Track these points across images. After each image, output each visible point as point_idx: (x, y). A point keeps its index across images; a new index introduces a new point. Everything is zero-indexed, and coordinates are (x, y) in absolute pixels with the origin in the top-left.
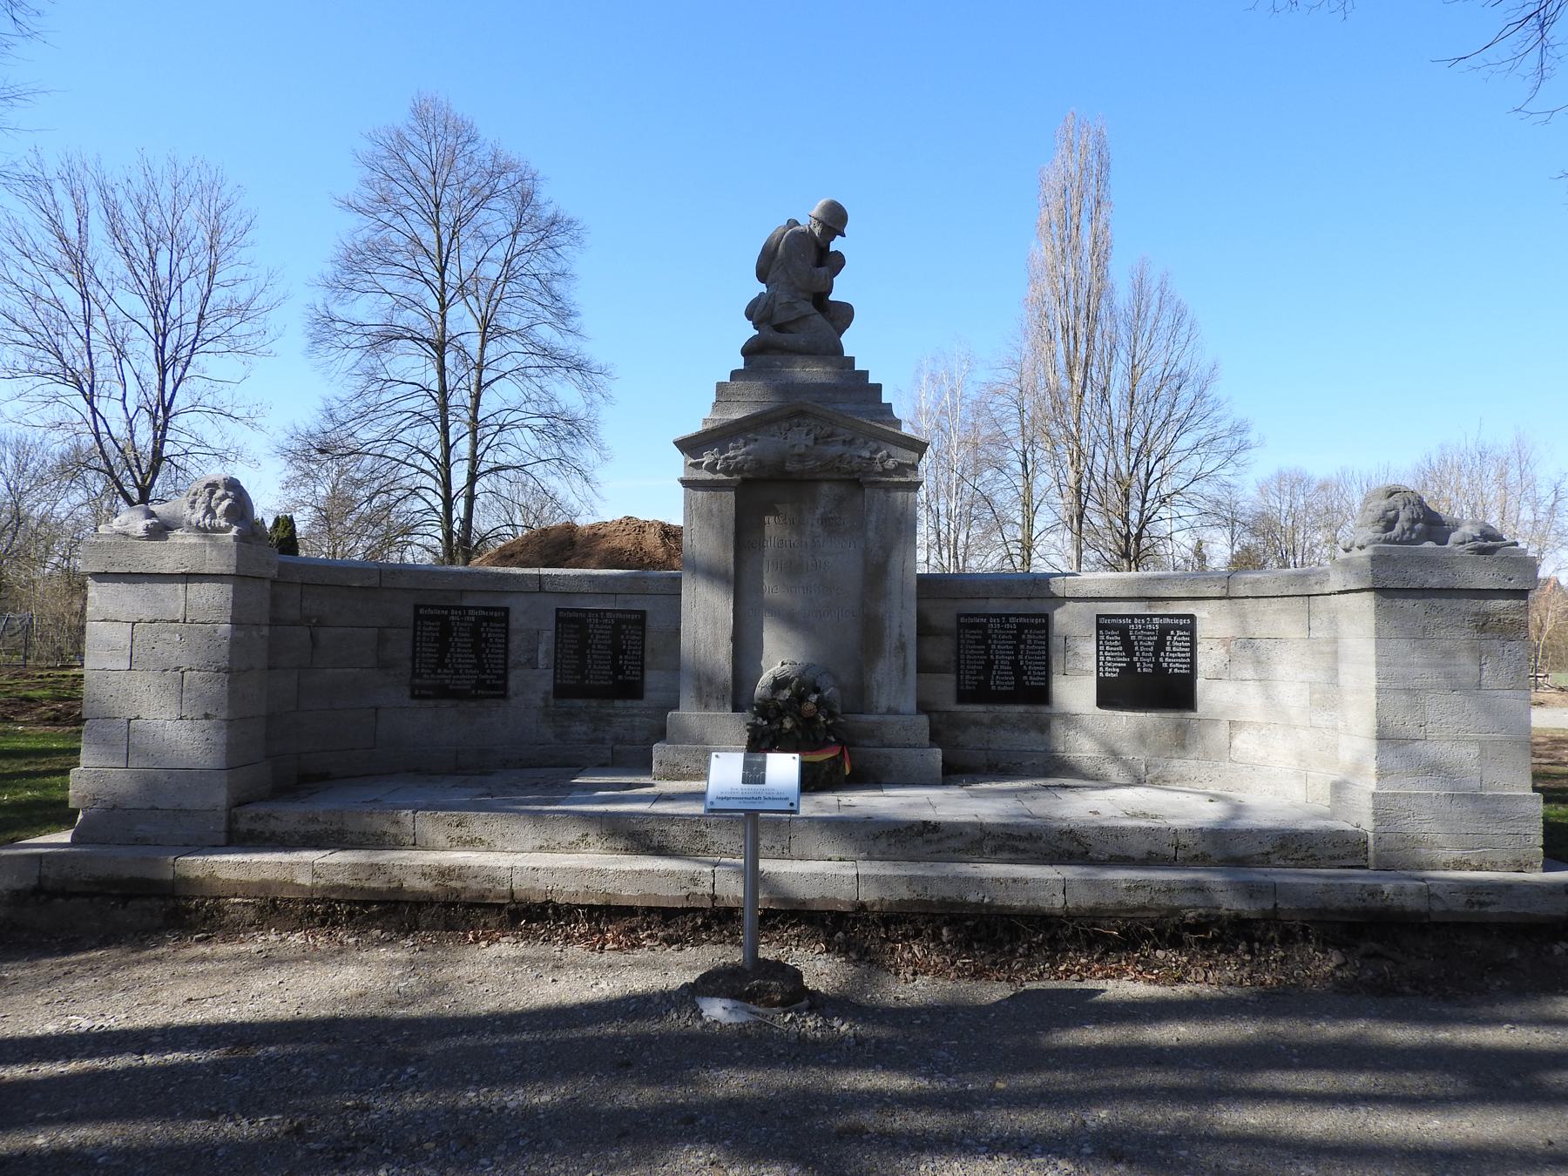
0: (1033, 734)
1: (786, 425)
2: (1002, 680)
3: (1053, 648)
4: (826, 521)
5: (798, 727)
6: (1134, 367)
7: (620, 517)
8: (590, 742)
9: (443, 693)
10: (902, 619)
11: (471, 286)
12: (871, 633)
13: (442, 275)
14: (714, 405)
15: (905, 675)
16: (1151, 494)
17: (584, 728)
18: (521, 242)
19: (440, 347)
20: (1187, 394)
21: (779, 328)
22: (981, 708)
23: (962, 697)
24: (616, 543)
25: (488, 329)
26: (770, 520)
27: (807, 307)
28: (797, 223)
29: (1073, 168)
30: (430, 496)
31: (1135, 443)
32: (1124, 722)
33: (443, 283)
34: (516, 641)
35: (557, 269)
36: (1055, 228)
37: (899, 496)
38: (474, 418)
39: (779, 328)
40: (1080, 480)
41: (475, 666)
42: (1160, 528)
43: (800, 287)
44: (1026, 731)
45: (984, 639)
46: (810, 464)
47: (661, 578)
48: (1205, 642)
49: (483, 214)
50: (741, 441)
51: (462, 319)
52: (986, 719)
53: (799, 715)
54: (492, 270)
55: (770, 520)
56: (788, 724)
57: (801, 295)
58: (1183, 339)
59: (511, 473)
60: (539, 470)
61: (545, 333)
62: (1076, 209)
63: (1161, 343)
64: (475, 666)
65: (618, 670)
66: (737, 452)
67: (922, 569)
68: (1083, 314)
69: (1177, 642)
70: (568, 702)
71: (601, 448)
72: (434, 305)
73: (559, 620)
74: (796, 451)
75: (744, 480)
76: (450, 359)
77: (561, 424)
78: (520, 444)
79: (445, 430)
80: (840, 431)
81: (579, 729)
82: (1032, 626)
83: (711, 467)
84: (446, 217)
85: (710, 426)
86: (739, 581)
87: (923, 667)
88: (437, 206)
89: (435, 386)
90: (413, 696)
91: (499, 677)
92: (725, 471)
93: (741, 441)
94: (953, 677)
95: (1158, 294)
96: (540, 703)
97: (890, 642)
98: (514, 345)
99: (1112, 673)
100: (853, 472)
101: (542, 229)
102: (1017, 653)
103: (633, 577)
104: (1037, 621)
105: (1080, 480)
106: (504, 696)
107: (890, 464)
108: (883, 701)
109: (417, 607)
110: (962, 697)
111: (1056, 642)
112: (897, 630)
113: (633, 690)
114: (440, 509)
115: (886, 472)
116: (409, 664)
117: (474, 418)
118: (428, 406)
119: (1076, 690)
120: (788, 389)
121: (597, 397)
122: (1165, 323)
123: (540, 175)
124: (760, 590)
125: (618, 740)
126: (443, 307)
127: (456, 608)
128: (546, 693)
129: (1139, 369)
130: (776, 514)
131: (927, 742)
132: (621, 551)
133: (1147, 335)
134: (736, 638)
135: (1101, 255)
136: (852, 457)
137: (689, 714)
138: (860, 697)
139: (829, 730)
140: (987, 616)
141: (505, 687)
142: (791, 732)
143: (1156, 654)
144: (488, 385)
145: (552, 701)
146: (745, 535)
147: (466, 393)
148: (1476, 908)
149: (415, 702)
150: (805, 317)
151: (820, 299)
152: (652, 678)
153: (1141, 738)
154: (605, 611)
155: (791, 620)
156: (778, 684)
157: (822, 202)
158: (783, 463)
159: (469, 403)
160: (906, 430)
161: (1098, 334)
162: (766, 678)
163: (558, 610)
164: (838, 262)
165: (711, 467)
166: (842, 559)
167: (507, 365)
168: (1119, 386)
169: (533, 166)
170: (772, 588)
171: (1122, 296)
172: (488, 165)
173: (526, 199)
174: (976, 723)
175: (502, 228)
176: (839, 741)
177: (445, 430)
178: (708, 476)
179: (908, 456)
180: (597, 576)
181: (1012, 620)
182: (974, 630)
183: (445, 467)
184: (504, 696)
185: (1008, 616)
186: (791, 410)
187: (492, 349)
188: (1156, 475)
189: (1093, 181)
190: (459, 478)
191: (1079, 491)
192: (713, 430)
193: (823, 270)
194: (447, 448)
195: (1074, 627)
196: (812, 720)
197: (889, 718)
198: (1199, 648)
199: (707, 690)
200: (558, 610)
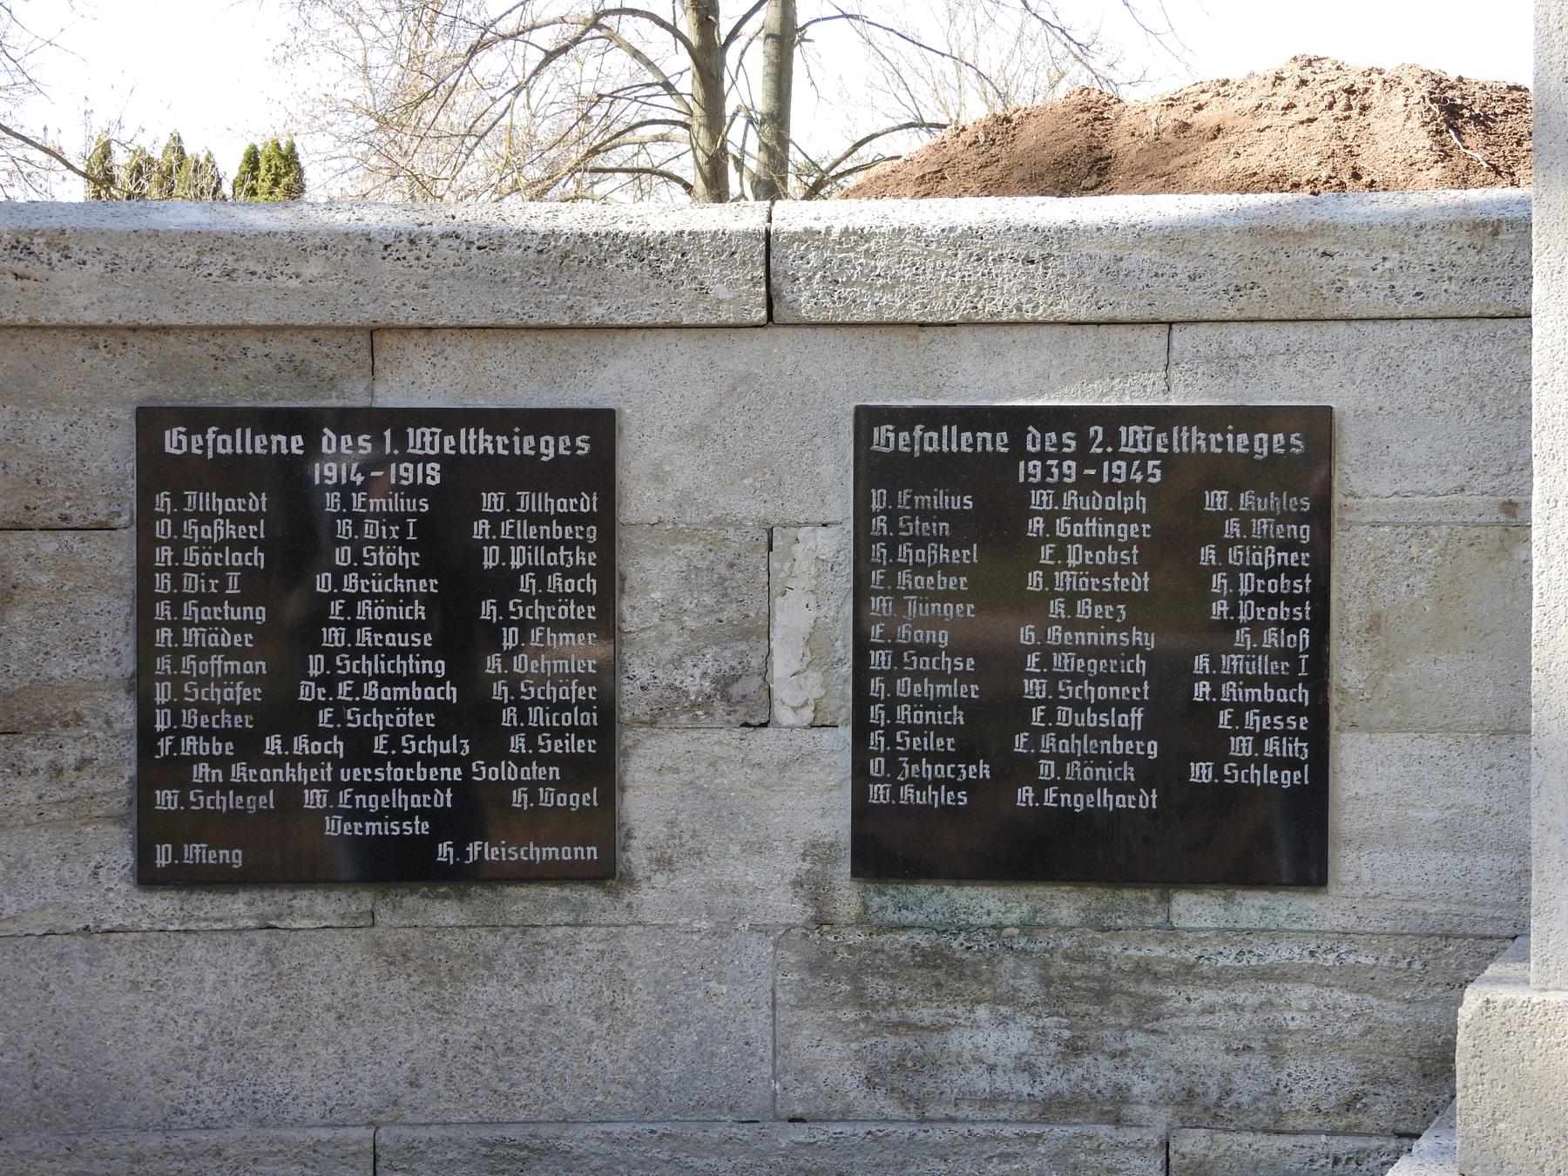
7: (1277, 59)
8: (1055, 1108)
9: (278, 855)
17: (1018, 1039)
34: (653, 585)
41: (447, 720)
64: (447, 720)
65: (1185, 724)
70: (937, 901)
73: (873, 470)
81: (992, 1041)
90: (148, 877)
91: (578, 772)
96: (795, 910)
104: (550, 448)
106: (605, 872)
109: (151, 421)
113: (1284, 839)
114: (687, 84)
116: (125, 712)
125: (1194, 1104)
127: (348, 420)
128: (816, 850)
141: (604, 826)
145: (847, 895)
149: (163, 904)
152: (1369, 775)
163: (867, 419)
181: (1133, 437)
184: (605, 872)
200: (867, 419)
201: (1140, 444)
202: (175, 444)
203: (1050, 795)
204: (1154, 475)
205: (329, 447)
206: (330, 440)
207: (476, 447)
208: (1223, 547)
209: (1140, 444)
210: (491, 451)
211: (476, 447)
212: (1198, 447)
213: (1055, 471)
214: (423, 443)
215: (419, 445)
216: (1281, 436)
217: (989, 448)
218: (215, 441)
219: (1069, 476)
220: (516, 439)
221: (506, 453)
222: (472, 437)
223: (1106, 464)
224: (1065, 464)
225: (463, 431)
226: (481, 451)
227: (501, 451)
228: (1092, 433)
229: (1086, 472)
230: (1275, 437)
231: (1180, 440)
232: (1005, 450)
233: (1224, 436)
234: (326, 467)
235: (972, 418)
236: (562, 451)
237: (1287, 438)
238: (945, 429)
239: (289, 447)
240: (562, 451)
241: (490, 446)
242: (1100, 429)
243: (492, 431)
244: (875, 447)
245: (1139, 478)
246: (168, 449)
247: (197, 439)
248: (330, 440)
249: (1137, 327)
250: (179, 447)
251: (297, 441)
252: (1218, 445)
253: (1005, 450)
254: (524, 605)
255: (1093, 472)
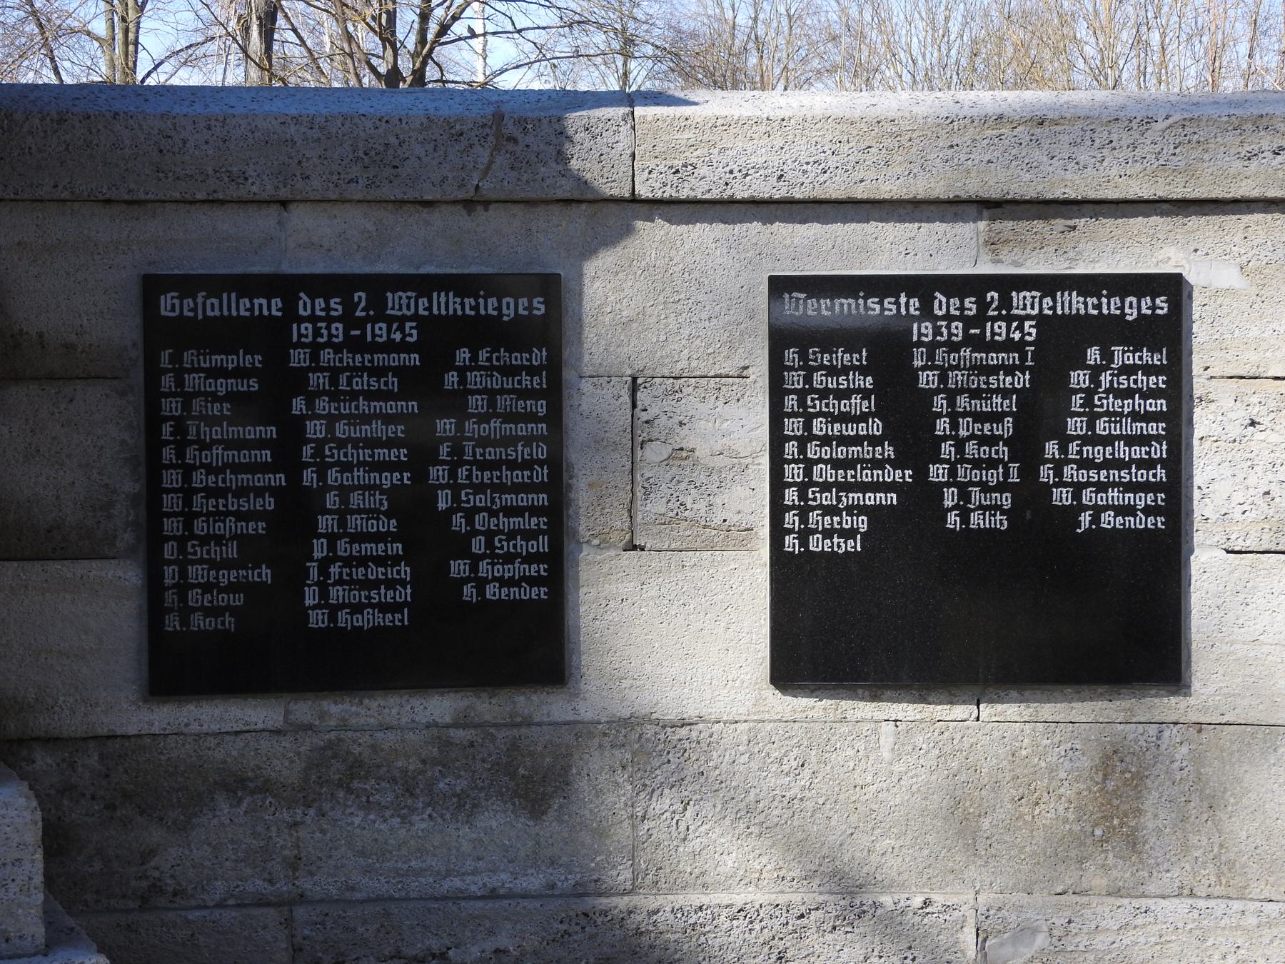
0: (498, 822)
2: (356, 592)
3: (578, 431)
22: (258, 713)
23: (179, 665)
32: (897, 755)
44: (464, 805)
45: (276, 393)
48: (1224, 393)
69: (1107, 389)
82: (1111, 331)
99: (838, 536)
102: (421, 457)
110: (179, 665)
111: (594, 403)
119: (681, 624)
140: (286, 286)
143: (1026, 448)
148: (314, 574)
153: (963, 820)
174: (237, 784)
181: (398, 302)
182: (233, 350)
185: (379, 285)
195: (672, 323)
198: (1203, 422)
201: (1029, 307)
202: (169, 308)
203: (342, 615)
204: (411, 335)
205: (305, 310)
206: (305, 304)
207: (1070, 308)
208: (311, 398)
209: (1029, 307)
210: (459, 312)
211: (1070, 308)
212: (1078, 310)
213: (945, 331)
214: (400, 305)
215: (397, 307)
216: (525, 300)
217: (265, 313)
218: (204, 304)
219: (337, 336)
220: (481, 301)
221: (473, 313)
222: (443, 300)
223: (369, 327)
224: (954, 325)
225: (435, 294)
226: (1074, 312)
227: (468, 312)
228: (356, 299)
229: (358, 332)
230: (520, 301)
231: (1063, 303)
232: (280, 314)
233: (1099, 299)
234: (377, 326)
235: (246, 285)
236: (521, 312)
237: (530, 302)
238: (225, 296)
239: (269, 309)
240: (1144, 311)
241: (459, 307)
242: (363, 295)
243: (1084, 293)
244: (389, 312)
245: (1017, 336)
246: (163, 313)
247: (188, 302)
248: (305, 304)
249: (516, 209)
250: (173, 309)
251: (277, 302)
252: (1094, 307)
253: (280, 314)
254: (339, 448)
255: (358, 332)
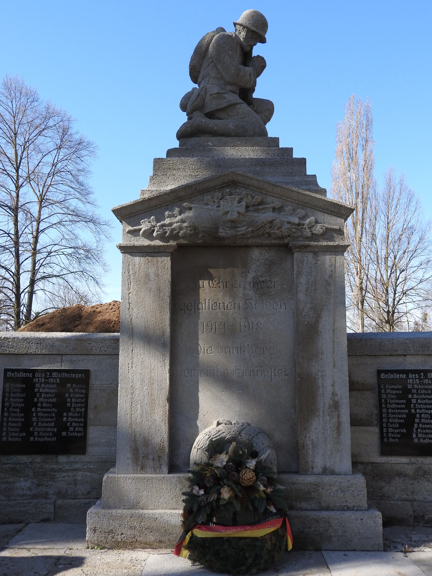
1: (218, 194)
4: (257, 284)
5: (236, 497)
6: (388, 223)
8: (35, 497)
10: (333, 376)
11: (32, 177)
12: (304, 393)
13: (17, 171)
14: (152, 179)
15: (339, 433)
16: (399, 289)
17: (28, 484)
18: (63, 152)
19: (15, 210)
20: (415, 238)
21: (210, 115)
22: (404, 460)
23: (386, 449)
24: (106, 317)
25: (42, 200)
26: (204, 284)
27: (235, 98)
28: (223, 30)
29: (354, 123)
30: (9, 293)
31: (390, 264)
33: (18, 176)
35: (80, 168)
36: (344, 154)
37: (328, 259)
38: (34, 249)
39: (210, 115)
40: (361, 283)
42: (401, 308)
43: (226, 83)
46: (242, 230)
47: (104, 340)
49: (41, 139)
50: (177, 210)
51: (29, 195)
52: (410, 470)
53: (237, 483)
54: (46, 170)
55: (204, 284)
56: (226, 494)
57: (229, 88)
58: (413, 209)
59: (54, 280)
60: (70, 278)
61: (74, 203)
62: (355, 143)
63: (401, 211)
66: (174, 220)
67: (349, 331)
68: (360, 196)
71: (105, 265)
72: (12, 187)
74: (229, 217)
75: (180, 247)
76: (21, 216)
77: (81, 251)
78: (59, 263)
79: (17, 256)
80: (269, 199)
83: (149, 234)
84: (20, 140)
85: (147, 196)
86: (176, 345)
87: (355, 422)
88: (15, 134)
89: (12, 232)
92: (162, 237)
93: (177, 210)
94: (376, 430)
95: (398, 187)
97: (324, 401)
98: (56, 209)
100: (282, 238)
101: (72, 146)
103: (78, 339)
105: (361, 283)
107: (318, 229)
108: (318, 462)
110: (386, 449)
112: (329, 389)
113: (75, 444)
114: (14, 300)
115: (315, 237)
117: (34, 249)
118: (10, 244)
120: (221, 164)
121: (103, 237)
122: (403, 201)
123: (72, 119)
124: (195, 350)
125: (61, 494)
126: (18, 188)
129: (391, 225)
130: (210, 278)
131: (364, 503)
132: (110, 321)
133: (394, 207)
134: (173, 399)
135: (368, 167)
136: (282, 222)
137: (124, 480)
138: (295, 457)
139: (269, 499)
142: (229, 502)
144: (43, 231)
146: (181, 299)
147: (30, 236)
150: (232, 105)
151: (246, 93)
152: (94, 433)
154: (51, 371)
155: (225, 381)
156: (216, 447)
157: (246, 12)
158: (217, 228)
159: (32, 241)
160: (330, 197)
161: (368, 207)
162: (201, 440)
163: (6, 371)
164: (260, 65)
165: (149, 234)
166: (275, 320)
167: (54, 220)
168: (380, 232)
169: (69, 114)
170: (208, 351)
171: (381, 188)
172: (44, 113)
173: (65, 131)
174: (400, 474)
175: (51, 146)
176: (281, 513)
177: (17, 256)
178: (146, 242)
179: (333, 222)
180: (44, 339)
183: (17, 275)
186: (224, 182)
187: (45, 212)
188: (400, 280)
189: (364, 130)
190: (25, 281)
191: (361, 289)
192: (150, 199)
193: (248, 69)
194: (18, 265)
196: (252, 488)
197: (327, 479)
199: (142, 455)
